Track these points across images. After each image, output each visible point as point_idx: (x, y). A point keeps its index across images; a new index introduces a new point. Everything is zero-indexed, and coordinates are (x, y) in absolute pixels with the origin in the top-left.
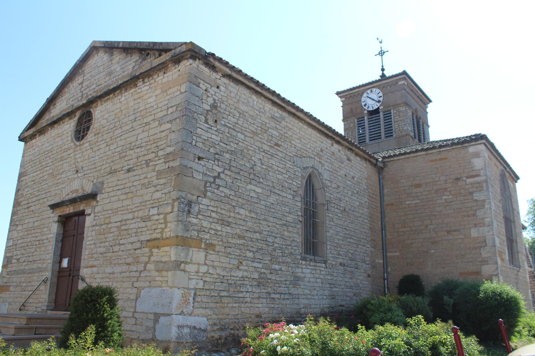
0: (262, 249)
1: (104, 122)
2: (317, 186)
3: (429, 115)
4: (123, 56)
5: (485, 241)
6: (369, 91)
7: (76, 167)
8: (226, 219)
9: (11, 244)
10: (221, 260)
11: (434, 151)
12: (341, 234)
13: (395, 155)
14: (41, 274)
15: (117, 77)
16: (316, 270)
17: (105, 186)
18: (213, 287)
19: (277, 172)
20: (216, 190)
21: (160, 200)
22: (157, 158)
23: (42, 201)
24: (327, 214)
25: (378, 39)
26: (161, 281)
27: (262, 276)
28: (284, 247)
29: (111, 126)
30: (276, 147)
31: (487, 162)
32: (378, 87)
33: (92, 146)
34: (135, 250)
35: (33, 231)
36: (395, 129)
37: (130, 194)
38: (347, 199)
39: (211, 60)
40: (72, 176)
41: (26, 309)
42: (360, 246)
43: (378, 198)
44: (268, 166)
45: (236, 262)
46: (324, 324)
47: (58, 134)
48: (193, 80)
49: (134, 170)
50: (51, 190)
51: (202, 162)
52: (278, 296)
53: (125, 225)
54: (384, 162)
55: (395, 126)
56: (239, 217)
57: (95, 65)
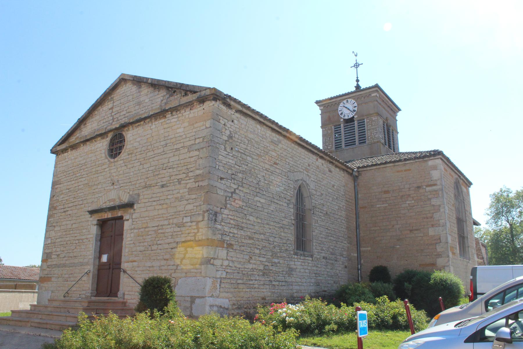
0: (265, 247)
1: (136, 144)
2: (305, 195)
3: (398, 123)
4: (151, 89)
5: (440, 239)
6: (345, 101)
7: (111, 180)
8: (240, 225)
9: (49, 242)
10: (238, 256)
11: (400, 163)
12: (324, 233)
13: (368, 166)
14: (82, 267)
15: (146, 107)
16: (305, 263)
17: (141, 197)
18: (232, 277)
19: (276, 186)
20: (233, 203)
21: (192, 211)
22: (188, 178)
23: (78, 207)
24: (313, 217)
25: (353, 52)
26: (196, 273)
27: (266, 267)
28: (281, 245)
29: (144, 149)
30: (275, 166)
31: (443, 173)
33: (126, 164)
34: (172, 249)
35: (71, 232)
36: (368, 137)
37: (165, 205)
38: (329, 204)
39: (228, 100)
40: (109, 188)
41: (70, 296)
42: (339, 243)
43: (354, 202)
44: (269, 181)
45: (247, 257)
46: (318, 303)
47: (91, 150)
48: (216, 117)
49: (168, 186)
50: (88, 198)
51: (223, 182)
52: (277, 283)
53: (161, 229)
54: (358, 172)
55: (368, 134)
56: (249, 222)
57: (124, 94)
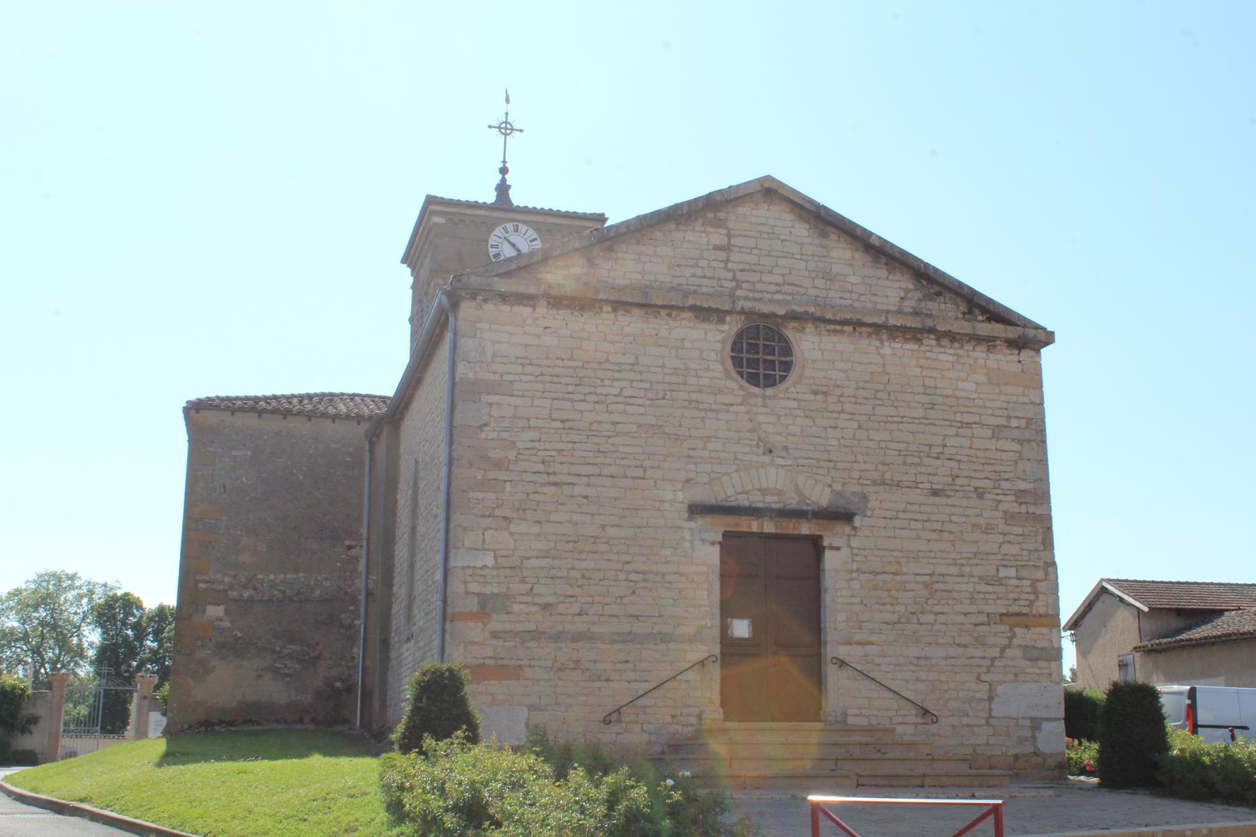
6: (510, 226)
32: (536, 226)
34: (976, 625)
49: (949, 496)
